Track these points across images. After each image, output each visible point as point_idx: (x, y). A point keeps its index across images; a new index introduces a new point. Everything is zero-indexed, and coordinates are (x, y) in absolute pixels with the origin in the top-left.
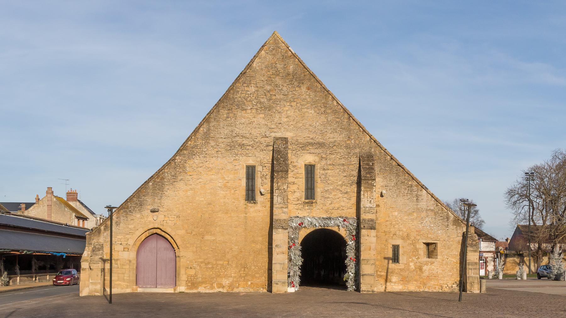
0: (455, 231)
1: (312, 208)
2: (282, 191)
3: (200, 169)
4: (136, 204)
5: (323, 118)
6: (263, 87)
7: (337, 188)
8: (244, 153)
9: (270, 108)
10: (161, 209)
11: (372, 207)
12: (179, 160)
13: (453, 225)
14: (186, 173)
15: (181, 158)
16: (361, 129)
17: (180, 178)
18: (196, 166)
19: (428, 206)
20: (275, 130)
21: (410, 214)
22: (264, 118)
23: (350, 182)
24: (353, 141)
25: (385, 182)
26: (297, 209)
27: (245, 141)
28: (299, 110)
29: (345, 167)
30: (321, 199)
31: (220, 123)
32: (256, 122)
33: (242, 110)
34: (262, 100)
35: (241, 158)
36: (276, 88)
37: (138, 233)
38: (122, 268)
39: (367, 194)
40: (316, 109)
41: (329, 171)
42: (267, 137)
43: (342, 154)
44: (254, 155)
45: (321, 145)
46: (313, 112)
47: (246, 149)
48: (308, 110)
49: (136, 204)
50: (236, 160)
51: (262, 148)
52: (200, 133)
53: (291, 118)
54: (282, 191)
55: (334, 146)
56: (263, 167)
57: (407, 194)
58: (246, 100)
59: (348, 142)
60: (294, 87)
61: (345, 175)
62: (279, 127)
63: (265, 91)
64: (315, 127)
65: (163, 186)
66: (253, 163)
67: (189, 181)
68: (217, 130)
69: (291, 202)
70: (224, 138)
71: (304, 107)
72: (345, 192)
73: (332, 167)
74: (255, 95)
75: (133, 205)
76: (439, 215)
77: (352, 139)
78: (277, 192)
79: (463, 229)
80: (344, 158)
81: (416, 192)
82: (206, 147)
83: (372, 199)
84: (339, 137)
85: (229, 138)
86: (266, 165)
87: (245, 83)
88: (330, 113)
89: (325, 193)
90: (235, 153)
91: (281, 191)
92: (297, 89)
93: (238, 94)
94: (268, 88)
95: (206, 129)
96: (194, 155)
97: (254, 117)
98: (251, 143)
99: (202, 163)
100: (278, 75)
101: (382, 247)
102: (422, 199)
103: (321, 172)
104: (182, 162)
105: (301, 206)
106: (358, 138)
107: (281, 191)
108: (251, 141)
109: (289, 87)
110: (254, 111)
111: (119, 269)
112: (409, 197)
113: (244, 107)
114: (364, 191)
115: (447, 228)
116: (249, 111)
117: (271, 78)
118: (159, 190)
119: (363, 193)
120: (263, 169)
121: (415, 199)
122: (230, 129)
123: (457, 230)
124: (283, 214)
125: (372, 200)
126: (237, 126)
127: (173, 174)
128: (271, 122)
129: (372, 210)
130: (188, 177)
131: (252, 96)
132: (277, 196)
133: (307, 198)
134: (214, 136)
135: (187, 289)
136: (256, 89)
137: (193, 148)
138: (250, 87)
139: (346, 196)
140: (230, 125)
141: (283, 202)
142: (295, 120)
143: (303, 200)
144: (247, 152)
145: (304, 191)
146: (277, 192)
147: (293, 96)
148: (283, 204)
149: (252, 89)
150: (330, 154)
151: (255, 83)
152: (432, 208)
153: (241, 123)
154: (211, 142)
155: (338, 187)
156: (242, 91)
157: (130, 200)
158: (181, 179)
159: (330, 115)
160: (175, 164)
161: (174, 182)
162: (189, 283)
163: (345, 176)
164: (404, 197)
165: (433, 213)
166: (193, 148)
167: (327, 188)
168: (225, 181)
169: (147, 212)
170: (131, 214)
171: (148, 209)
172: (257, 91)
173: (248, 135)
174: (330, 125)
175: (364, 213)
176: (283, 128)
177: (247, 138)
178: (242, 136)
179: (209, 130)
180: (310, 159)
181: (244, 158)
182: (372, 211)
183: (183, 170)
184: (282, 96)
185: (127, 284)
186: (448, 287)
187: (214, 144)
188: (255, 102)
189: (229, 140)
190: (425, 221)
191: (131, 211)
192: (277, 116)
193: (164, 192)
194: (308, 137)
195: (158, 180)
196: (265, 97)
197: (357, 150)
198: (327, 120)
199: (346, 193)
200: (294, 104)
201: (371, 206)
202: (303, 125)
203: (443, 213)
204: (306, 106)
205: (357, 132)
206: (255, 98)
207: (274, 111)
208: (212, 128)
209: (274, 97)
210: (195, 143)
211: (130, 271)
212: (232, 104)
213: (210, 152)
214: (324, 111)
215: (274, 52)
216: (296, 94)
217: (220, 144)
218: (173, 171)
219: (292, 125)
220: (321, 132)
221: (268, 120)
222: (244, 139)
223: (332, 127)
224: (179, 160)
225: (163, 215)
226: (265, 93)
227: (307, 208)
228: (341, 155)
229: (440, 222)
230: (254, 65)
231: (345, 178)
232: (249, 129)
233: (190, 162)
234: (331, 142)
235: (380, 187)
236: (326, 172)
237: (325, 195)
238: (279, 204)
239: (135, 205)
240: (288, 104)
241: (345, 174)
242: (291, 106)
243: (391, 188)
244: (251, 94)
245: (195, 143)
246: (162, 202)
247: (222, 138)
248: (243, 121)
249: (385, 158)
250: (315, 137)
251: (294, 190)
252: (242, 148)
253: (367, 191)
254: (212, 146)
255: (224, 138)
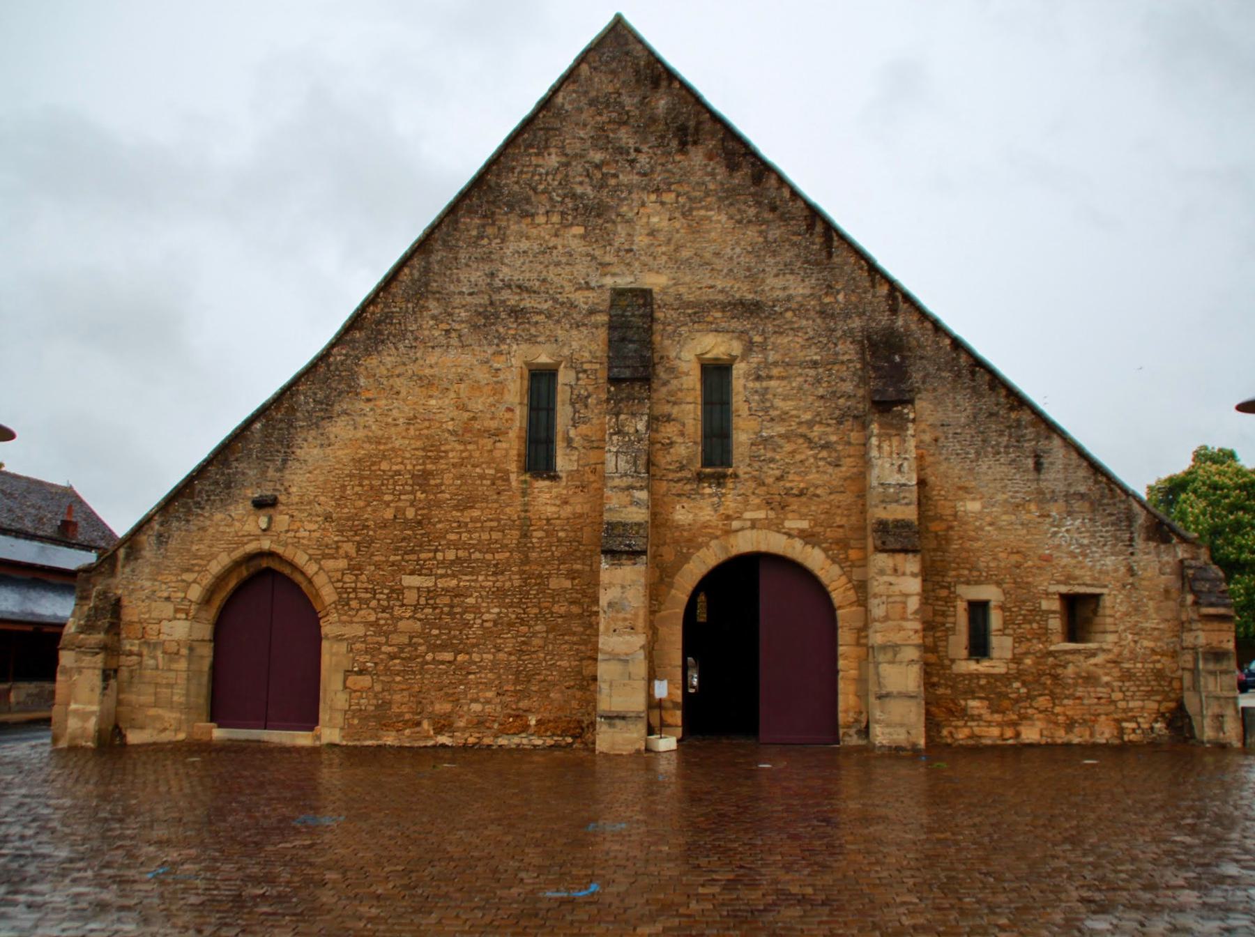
0: (1152, 557)
1: (724, 491)
2: (630, 440)
3: (398, 382)
4: (217, 483)
5: (751, 233)
6: (582, 156)
7: (800, 430)
8: (523, 334)
9: (600, 210)
10: (282, 498)
11: (905, 485)
12: (338, 358)
13: (1148, 539)
14: (357, 394)
15: (344, 352)
16: (863, 262)
17: (337, 408)
18: (385, 372)
19: (1070, 485)
20: (616, 270)
21: (385, 526)
22: (583, 237)
23: (837, 412)
24: (841, 297)
25: (939, 415)
26: (679, 495)
27: (528, 300)
28: (684, 215)
29: (821, 370)
30: (749, 465)
31: (458, 252)
32: (560, 247)
33: (522, 217)
34: (579, 190)
35: (515, 347)
36: (618, 157)
37: (215, 568)
38: (170, 670)
39: (891, 446)
40: (732, 210)
41: (773, 383)
42: (593, 289)
43: (811, 333)
44: (553, 339)
45: (751, 308)
46: (723, 218)
47: (529, 323)
48: (711, 213)
49: (217, 483)
50: (501, 353)
51: (578, 318)
52: (402, 282)
53: (662, 237)
54: (632, 438)
55: (787, 310)
56: (578, 373)
57: (1006, 447)
58: (535, 190)
59: (827, 300)
60: (670, 154)
61: (821, 391)
62: (627, 261)
63: (587, 165)
64: (731, 259)
65: (292, 431)
66: (549, 361)
67: (365, 415)
68: (448, 272)
69: (659, 474)
70: (471, 294)
71: (699, 205)
72: (823, 442)
73: (781, 369)
74: (559, 177)
75: (207, 488)
76: (1104, 510)
77: (838, 292)
78: (615, 442)
79: (1176, 553)
80: (815, 344)
81: (1034, 443)
82: (416, 320)
83: (905, 459)
84: (799, 288)
85: (482, 292)
86: (586, 366)
87: (531, 146)
88: (774, 221)
89: (761, 447)
90: (496, 335)
91: (627, 439)
92: (678, 158)
93: (510, 175)
94: (598, 157)
95: (419, 270)
96: (383, 342)
97: (556, 235)
98: (545, 306)
99: (404, 364)
100: (625, 123)
101: (937, 608)
102: (1052, 463)
103: (751, 385)
104: (349, 362)
105: (688, 487)
106: (857, 287)
107: (627, 439)
108: (546, 301)
109: (656, 155)
110: (555, 218)
111: (159, 672)
112: (1013, 455)
113: (527, 207)
114: (879, 436)
115: (1131, 550)
116: (541, 219)
117: (604, 131)
118: (280, 441)
119: (877, 443)
120: (578, 379)
121: (1030, 462)
122: (487, 267)
123: (1158, 555)
124: (634, 509)
125: (906, 464)
126: (506, 261)
127: (320, 395)
128: (605, 246)
129: (907, 495)
130: (362, 405)
131: (550, 178)
132: (617, 452)
133: (707, 462)
134: (439, 289)
135: (343, 737)
136: (564, 160)
137: (379, 323)
138: (546, 154)
139: (824, 454)
140: (487, 258)
141: (633, 469)
142: (673, 241)
143: (698, 465)
144: (533, 331)
145: (699, 440)
146: (615, 442)
147: (667, 175)
148: (632, 477)
149: (553, 160)
150: (775, 332)
151: (560, 145)
152: (1083, 489)
153: (518, 252)
154: (431, 307)
155: (803, 430)
156: (524, 166)
157: (201, 472)
158: (345, 413)
159: (773, 226)
160: (329, 369)
161: (323, 419)
162: (353, 717)
163: (822, 397)
164: (998, 457)
165: (1087, 505)
166: (379, 323)
167: (769, 431)
168: (466, 415)
169: (241, 509)
170: (199, 511)
171: (245, 498)
172: (567, 165)
173: (537, 283)
174: (774, 254)
175: (883, 501)
176: (637, 264)
177: (535, 292)
178: (519, 287)
179: (427, 270)
180: (715, 345)
181: (524, 346)
182: (904, 498)
183: (350, 387)
184: (636, 177)
185: (178, 715)
186: (1138, 731)
187: (440, 310)
188: (558, 195)
189: (484, 300)
190: (1064, 529)
191: (199, 503)
192: (621, 230)
193: (294, 449)
194: (711, 287)
195: (279, 416)
196: (587, 180)
197: (856, 323)
198: (766, 238)
199: (827, 446)
200: (669, 198)
201: (903, 481)
202: (695, 254)
203: (1115, 504)
204: (703, 203)
205: (853, 272)
206: (560, 184)
207: (613, 217)
208: (436, 267)
209: (613, 182)
210: (386, 310)
211: (188, 679)
212: (493, 203)
213: (426, 333)
214: (757, 216)
215: (614, 65)
216: (675, 170)
217: (457, 311)
218: (321, 389)
219: (663, 253)
220: (748, 274)
221: (597, 241)
222: (525, 295)
223: (778, 259)
224: (338, 358)
225: (287, 514)
226: (588, 171)
227: (708, 491)
228: (807, 337)
229: (1107, 531)
230: (559, 99)
231: (822, 402)
232: (540, 267)
233: (373, 362)
234: (778, 300)
235: (927, 429)
236: (765, 384)
237: (762, 451)
238: (621, 477)
239: (212, 488)
240: (653, 197)
241: (821, 389)
242: (663, 203)
243: (959, 431)
244: (547, 174)
245: (386, 310)
246: (287, 476)
247: (461, 293)
248: (524, 245)
249: (938, 343)
250: (732, 288)
251: (669, 438)
252: (520, 321)
253: (889, 436)
254: (434, 317)
255: (471, 294)
